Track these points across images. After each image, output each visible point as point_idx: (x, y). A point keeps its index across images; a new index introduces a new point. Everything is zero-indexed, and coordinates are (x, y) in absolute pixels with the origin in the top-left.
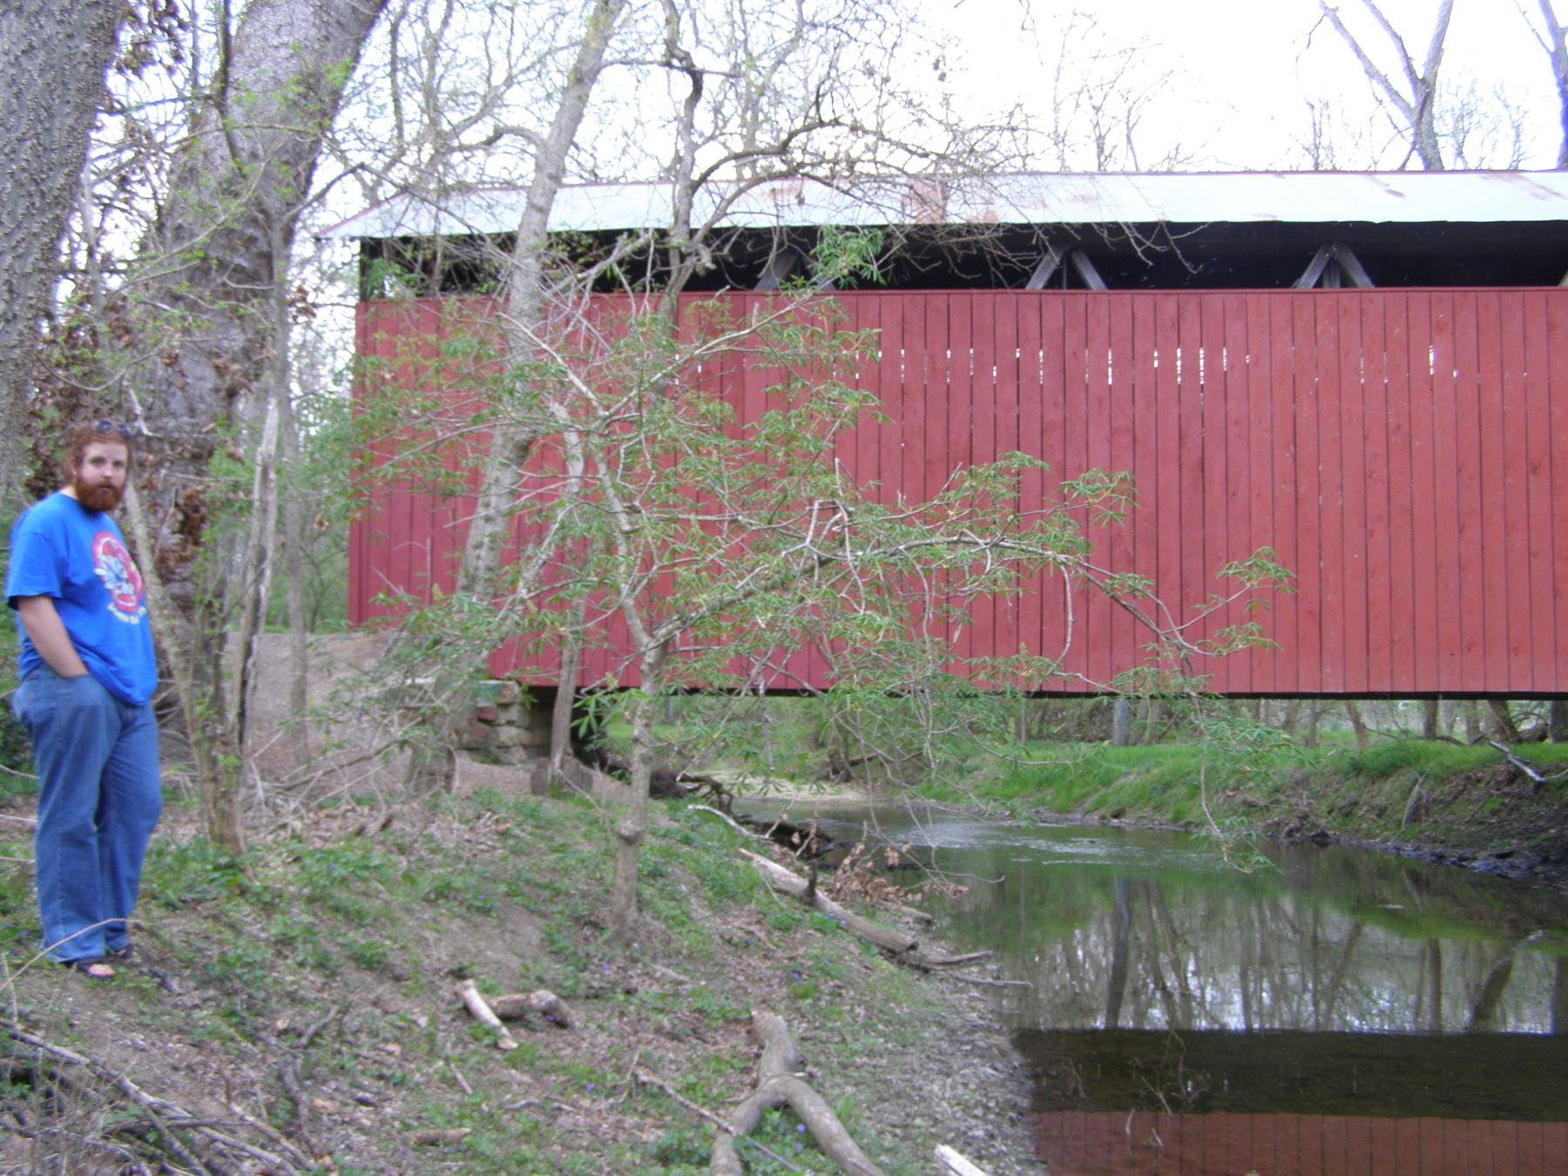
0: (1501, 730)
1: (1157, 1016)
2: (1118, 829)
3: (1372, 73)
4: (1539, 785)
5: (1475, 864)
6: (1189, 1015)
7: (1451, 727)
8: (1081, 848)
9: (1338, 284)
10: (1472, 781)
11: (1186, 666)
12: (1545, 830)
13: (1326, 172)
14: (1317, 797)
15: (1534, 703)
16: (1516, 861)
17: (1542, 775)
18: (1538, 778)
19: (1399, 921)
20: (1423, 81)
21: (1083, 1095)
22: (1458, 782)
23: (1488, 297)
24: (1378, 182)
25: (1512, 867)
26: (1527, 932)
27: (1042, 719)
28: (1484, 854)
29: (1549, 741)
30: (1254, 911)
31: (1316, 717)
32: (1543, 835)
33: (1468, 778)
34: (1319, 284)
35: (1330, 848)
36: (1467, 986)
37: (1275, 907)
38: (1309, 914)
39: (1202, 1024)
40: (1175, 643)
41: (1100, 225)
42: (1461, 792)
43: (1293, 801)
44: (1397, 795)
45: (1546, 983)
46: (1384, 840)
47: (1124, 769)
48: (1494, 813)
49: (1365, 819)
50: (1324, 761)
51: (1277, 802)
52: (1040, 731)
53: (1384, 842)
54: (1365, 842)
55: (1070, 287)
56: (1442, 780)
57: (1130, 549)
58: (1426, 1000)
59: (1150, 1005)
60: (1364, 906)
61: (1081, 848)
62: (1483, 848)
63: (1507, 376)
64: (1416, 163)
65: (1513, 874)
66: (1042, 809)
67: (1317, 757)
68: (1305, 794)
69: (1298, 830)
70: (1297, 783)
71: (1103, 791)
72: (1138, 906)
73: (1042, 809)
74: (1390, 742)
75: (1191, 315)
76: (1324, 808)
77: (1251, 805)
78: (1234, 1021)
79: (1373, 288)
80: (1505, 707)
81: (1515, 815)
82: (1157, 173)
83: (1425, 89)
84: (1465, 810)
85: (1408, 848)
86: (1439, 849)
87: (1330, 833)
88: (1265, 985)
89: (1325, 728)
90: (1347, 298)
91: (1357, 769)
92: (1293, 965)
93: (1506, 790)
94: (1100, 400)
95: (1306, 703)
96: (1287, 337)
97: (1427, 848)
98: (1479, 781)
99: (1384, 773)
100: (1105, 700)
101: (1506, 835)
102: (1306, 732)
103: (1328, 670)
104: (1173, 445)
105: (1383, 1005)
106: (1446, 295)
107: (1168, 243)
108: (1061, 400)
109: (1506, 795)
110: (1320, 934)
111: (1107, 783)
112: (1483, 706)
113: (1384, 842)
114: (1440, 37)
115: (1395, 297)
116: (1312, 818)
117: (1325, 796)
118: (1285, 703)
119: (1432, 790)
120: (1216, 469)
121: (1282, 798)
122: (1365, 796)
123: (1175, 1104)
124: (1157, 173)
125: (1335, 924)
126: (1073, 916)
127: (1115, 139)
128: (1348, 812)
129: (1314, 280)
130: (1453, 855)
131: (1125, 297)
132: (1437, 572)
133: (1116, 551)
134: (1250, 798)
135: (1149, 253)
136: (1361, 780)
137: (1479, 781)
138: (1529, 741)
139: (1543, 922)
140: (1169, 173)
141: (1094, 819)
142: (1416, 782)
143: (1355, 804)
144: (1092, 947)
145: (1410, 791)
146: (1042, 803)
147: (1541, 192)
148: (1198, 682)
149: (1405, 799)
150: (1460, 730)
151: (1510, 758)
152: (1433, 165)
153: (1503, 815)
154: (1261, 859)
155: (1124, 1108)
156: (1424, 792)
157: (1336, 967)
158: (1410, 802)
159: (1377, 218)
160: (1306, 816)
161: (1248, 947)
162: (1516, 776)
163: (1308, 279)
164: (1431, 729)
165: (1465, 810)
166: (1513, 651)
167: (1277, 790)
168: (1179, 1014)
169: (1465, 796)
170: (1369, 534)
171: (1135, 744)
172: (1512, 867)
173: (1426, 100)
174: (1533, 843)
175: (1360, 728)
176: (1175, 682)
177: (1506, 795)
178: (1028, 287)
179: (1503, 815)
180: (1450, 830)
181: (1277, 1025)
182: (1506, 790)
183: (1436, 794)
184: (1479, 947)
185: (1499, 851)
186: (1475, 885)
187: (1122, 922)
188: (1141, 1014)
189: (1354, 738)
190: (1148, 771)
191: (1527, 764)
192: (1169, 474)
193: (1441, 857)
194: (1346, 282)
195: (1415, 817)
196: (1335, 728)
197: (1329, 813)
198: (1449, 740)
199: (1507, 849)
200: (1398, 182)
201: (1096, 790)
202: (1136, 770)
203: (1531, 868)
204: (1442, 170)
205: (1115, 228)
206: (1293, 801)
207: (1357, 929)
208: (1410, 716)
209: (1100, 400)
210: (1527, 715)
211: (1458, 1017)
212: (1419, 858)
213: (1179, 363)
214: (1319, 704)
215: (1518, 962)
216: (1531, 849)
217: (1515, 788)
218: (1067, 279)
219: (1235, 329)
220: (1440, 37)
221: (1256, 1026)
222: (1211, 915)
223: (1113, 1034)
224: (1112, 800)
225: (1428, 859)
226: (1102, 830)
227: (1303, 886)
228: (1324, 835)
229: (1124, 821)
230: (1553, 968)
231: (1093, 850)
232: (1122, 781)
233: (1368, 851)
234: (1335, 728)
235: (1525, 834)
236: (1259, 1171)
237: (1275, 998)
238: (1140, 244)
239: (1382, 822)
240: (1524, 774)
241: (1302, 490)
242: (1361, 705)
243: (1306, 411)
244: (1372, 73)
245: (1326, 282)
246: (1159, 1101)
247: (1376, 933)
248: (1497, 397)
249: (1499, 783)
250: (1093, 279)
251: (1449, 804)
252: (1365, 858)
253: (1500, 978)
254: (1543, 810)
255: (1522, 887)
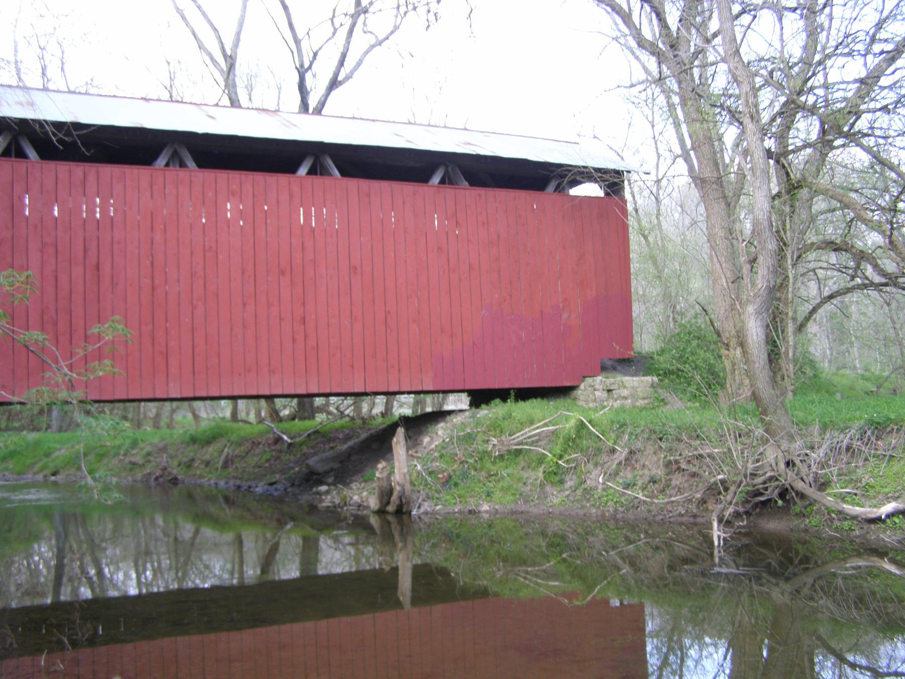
0: (271, 416)
1: (86, 593)
2: (55, 483)
3: (201, 46)
4: (290, 445)
5: (257, 489)
6: (103, 590)
7: (248, 414)
8: (32, 495)
9: (178, 164)
10: (255, 444)
11: (71, 386)
12: (292, 468)
13: (177, 101)
14: (172, 457)
15: (289, 400)
16: (279, 486)
17: (291, 439)
18: (289, 441)
19: (218, 523)
20: (231, 57)
21: (15, 646)
22: (248, 445)
23: (260, 178)
24: (203, 110)
25: (276, 490)
26: (286, 524)
27: (8, 419)
28: (262, 484)
29: (297, 420)
30: (140, 525)
31: (173, 411)
32: (292, 472)
33: (254, 443)
34: (167, 165)
35: (180, 485)
36: (259, 557)
37: (152, 520)
38: (172, 525)
39: (113, 593)
40: (61, 372)
41: (34, 121)
42: (250, 451)
43: (158, 460)
44: (216, 454)
45: (297, 551)
46: (210, 479)
47: (58, 446)
48: (267, 461)
49: (199, 468)
50: (175, 437)
51: (149, 461)
52: (7, 425)
53: (209, 480)
54: (199, 481)
55: (16, 156)
56: (239, 444)
57: (54, 316)
58: (237, 566)
59: (80, 584)
60: (201, 517)
61: (32, 495)
62: (261, 480)
63: (268, 221)
64: (226, 101)
65: (276, 494)
66: (6, 473)
67: (171, 434)
68: (165, 456)
69: (161, 476)
70: (160, 450)
71: (45, 460)
72: (72, 528)
73: (6, 473)
74: (213, 424)
75: (92, 178)
76: (176, 463)
77: (134, 464)
78: (133, 591)
79: (197, 169)
80: (273, 403)
81: (278, 461)
82: (80, 93)
83: (231, 61)
84: (253, 460)
85: (222, 483)
86: (238, 482)
87: (179, 477)
88: (149, 566)
89: (178, 417)
90: (182, 174)
91: (194, 440)
92: (164, 553)
93: (273, 448)
94: (36, 226)
95: (167, 404)
96: (148, 194)
97: (232, 483)
98: (259, 443)
99: (208, 442)
100: (18, 407)
101: (273, 473)
102: (167, 421)
103: (171, 385)
104: (81, 254)
105: (214, 570)
106: (237, 176)
107: (72, 136)
108: (10, 226)
109: (273, 450)
110: (178, 534)
111: (47, 455)
112: (263, 402)
113: (209, 480)
114: (238, 34)
115: (209, 175)
116: (169, 469)
117: (176, 456)
118: (156, 404)
119: (234, 450)
120: (106, 268)
121: (152, 458)
122: (198, 456)
123: (75, 644)
124: (80, 93)
125: (187, 530)
126: (36, 537)
127: (53, 71)
128: (189, 465)
129: (164, 163)
130: (245, 485)
131: (51, 165)
132: (231, 329)
133: (45, 317)
134: (133, 459)
135: (60, 141)
136: (196, 446)
137: (259, 443)
138: (286, 421)
139: (293, 518)
140: (86, 94)
141: (40, 477)
142: (226, 446)
143: (193, 460)
144: (43, 553)
145: (223, 451)
146: (7, 469)
147: (287, 124)
148: (79, 394)
149: (220, 456)
150: (252, 418)
151: (275, 430)
152: (234, 103)
153: (272, 462)
154: (117, 495)
155: (40, 651)
156: (230, 452)
157: (184, 553)
158: (223, 457)
159: (200, 130)
160: (165, 469)
161: (138, 546)
162: (278, 440)
163: (161, 162)
164: (234, 416)
165: (253, 460)
166: (272, 372)
167: (149, 454)
168: (98, 590)
169: (252, 452)
170: (194, 307)
171: (66, 431)
172: (276, 490)
173: (231, 67)
174: (287, 476)
175: (196, 417)
176: (63, 395)
177: (273, 450)
178: (430, 183)
179: (272, 462)
180: (244, 471)
181: (155, 590)
182: (273, 448)
183: (237, 452)
184: (264, 536)
185: (269, 481)
186: (258, 501)
187: (62, 538)
188: (75, 591)
189: (193, 422)
190: (73, 447)
191: (283, 433)
192: (78, 271)
193: (239, 487)
194: (182, 165)
195: (225, 465)
196: (184, 417)
197: (179, 465)
198: (246, 422)
199: (274, 480)
200: (213, 111)
201: (41, 460)
202: (66, 446)
203: (285, 489)
204: (240, 107)
205: (40, 123)
206: (158, 460)
207: (197, 532)
208: (225, 409)
209: (36, 226)
210: (285, 407)
211: (252, 572)
212: (227, 488)
213: (27, 201)
214: (175, 404)
215: (283, 541)
216: (286, 479)
217: (278, 447)
218: (176, 160)
219: (118, 188)
220: (238, 34)
221: (144, 591)
222: (115, 530)
223: (57, 606)
224: (51, 465)
225: (233, 488)
226: (45, 484)
227: (166, 509)
228: (176, 479)
229: (59, 478)
230: (301, 542)
231: (42, 496)
232: (57, 454)
233: (201, 486)
234: (184, 417)
235: (282, 472)
236: (122, 675)
237: (155, 575)
238: (55, 135)
239: (208, 469)
240: (282, 439)
241: (156, 282)
242: (198, 404)
243: (158, 237)
244: (201, 46)
245: (171, 164)
246: (63, 643)
247: (208, 532)
248: (263, 234)
249: (269, 444)
250: (32, 154)
251: (243, 458)
252: (199, 490)
253: (274, 549)
254: (292, 458)
255: (280, 500)
